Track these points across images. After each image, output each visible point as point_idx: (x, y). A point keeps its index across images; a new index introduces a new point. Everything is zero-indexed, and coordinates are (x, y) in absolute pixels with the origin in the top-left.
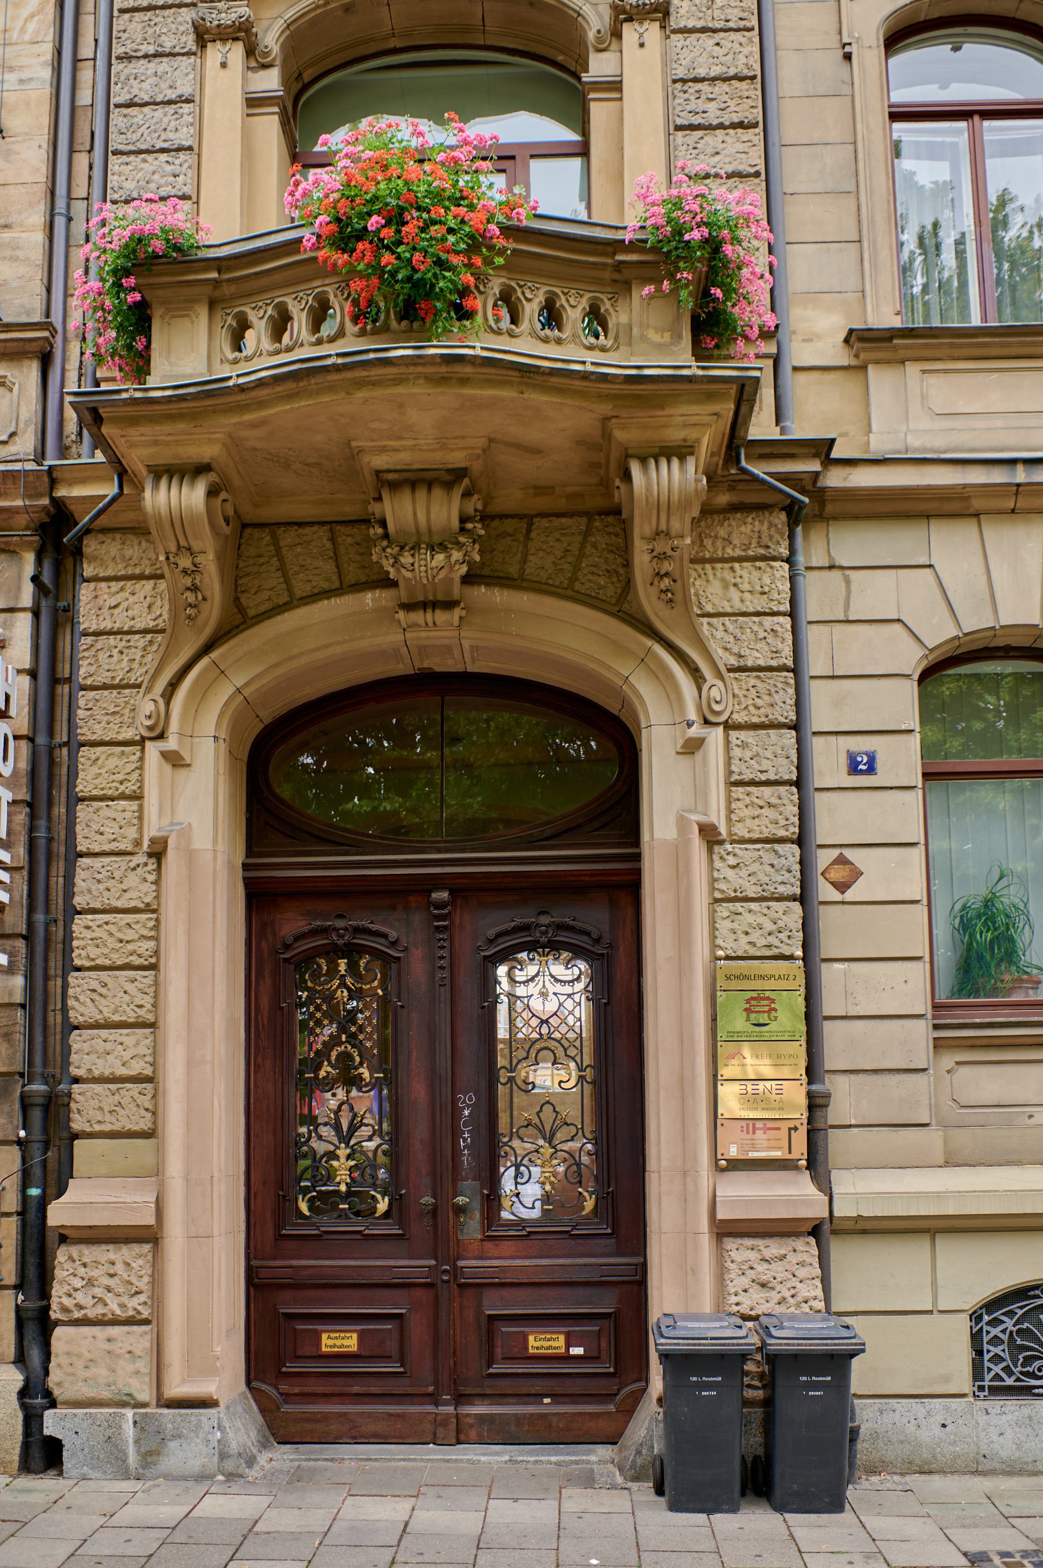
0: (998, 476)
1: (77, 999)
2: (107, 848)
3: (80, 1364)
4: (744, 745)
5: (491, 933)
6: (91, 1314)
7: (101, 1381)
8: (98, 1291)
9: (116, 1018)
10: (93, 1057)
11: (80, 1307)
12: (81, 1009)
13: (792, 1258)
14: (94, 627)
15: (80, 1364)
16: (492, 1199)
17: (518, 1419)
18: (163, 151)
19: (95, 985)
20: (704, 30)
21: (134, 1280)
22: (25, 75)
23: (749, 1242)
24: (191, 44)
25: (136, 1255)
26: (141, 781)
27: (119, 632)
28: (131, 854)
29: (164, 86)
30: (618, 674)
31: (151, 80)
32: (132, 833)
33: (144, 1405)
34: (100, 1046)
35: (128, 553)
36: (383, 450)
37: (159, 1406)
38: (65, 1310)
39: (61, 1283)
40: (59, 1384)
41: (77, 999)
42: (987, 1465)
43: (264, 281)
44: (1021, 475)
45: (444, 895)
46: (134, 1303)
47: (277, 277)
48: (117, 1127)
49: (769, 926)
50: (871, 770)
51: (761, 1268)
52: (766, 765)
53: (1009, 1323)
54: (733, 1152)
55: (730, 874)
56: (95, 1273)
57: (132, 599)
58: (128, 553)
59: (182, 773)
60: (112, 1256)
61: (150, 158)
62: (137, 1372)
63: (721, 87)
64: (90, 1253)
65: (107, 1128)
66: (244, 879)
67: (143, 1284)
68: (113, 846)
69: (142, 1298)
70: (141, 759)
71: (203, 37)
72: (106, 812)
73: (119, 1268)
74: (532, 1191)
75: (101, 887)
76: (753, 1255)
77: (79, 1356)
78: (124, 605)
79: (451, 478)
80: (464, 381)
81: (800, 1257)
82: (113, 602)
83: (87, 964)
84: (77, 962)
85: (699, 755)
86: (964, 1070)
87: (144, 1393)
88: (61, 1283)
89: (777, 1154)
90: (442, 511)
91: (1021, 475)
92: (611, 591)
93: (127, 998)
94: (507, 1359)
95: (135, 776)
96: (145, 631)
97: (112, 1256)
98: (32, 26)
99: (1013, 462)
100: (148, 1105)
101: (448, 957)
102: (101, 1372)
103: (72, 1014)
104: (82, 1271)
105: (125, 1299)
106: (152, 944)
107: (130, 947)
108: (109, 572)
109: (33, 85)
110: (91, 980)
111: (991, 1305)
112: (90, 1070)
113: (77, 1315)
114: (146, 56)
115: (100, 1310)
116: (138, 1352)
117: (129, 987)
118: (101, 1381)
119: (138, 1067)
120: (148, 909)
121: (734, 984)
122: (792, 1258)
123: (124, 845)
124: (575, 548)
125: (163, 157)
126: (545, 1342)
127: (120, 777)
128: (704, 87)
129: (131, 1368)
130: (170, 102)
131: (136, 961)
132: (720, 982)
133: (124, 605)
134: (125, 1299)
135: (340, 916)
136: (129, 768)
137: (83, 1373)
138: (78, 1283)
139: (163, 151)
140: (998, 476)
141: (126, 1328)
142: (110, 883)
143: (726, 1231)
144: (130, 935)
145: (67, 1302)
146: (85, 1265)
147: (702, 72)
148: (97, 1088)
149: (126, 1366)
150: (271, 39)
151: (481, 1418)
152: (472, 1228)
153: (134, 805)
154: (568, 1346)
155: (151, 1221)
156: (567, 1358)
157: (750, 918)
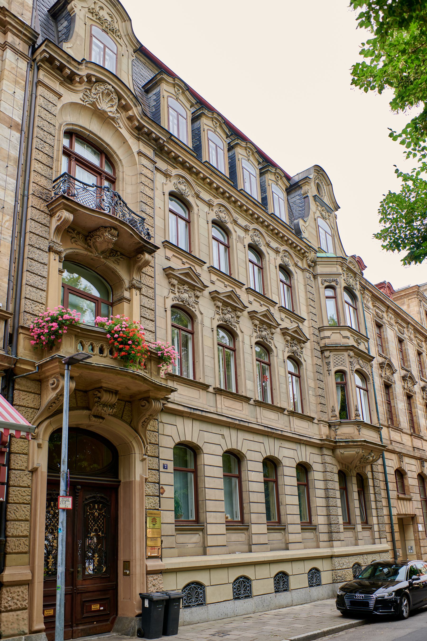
0: (189, 410)
1: (10, 512)
2: (19, 468)
3: (9, 624)
4: (150, 460)
5: (87, 497)
6: (13, 608)
7: (16, 628)
8: (15, 601)
9: (20, 518)
10: (13, 530)
11: (10, 606)
12: (11, 515)
13: (159, 579)
14: (18, 404)
15: (9, 624)
16: (84, 569)
17: (90, 629)
18: (39, 276)
19: (15, 508)
20: (146, 296)
21: (24, 596)
22: (5, 237)
23: (151, 576)
24: (47, 250)
25: (24, 589)
26: (28, 450)
27: (24, 407)
28: (24, 470)
29: (41, 258)
30: (129, 440)
31: (37, 255)
32: (25, 464)
33: (26, 634)
34: (16, 527)
35: (28, 385)
36: (106, 383)
37: (30, 634)
38: (5, 607)
39: (4, 599)
40: (4, 631)
41: (10, 512)
42: (185, 623)
43: (90, 336)
44: (192, 411)
45: (80, 487)
46: (25, 603)
47: (93, 337)
48: (19, 551)
49: (154, 502)
50: (167, 468)
51: (154, 581)
52: (154, 465)
53: (187, 591)
54: (149, 554)
55: (148, 489)
56: (14, 595)
57: (28, 398)
58: (28, 385)
59: (40, 449)
60: (18, 590)
61: (37, 276)
62: (25, 624)
63: (149, 311)
64: (13, 589)
65: (16, 551)
66: (48, 480)
67: (27, 597)
68: (21, 468)
69: (27, 601)
70: (28, 444)
71: (50, 249)
72: (19, 458)
73: (21, 593)
74: (91, 567)
75: (18, 479)
76: (152, 579)
77: (9, 621)
78: (27, 399)
79: (116, 393)
80: (136, 379)
81: (160, 578)
82: (23, 397)
83: (13, 502)
84: (10, 501)
85: (144, 462)
86: (178, 535)
87: (27, 631)
88: (4, 599)
89: (156, 555)
90: (113, 399)
91: (192, 411)
92: (129, 420)
93: (23, 513)
94: (87, 612)
95: (27, 448)
96: (31, 408)
97: (18, 590)
98: (7, 224)
99: (191, 408)
100: (28, 544)
101: (407, 550)
102: (16, 626)
103: (8, 516)
104: (10, 595)
105: (22, 602)
106: (30, 497)
107: (24, 498)
108: (22, 389)
109: (6, 241)
110: (14, 507)
111: (184, 588)
112: (12, 534)
113: (9, 609)
114: (36, 248)
115: (15, 606)
116: (25, 618)
117: (24, 509)
118: (16, 628)
119: (26, 533)
120: (29, 487)
121: (150, 515)
122: (159, 579)
123: (23, 468)
124: (123, 408)
125: (40, 277)
126: (95, 607)
127: (23, 448)
128: (146, 309)
129: (23, 623)
130: (42, 263)
131: (26, 502)
132: (148, 515)
133: (27, 399)
134: (22, 602)
135: (55, 490)
136: (25, 446)
137: (10, 627)
138: (9, 599)
139: (39, 276)
140: (189, 410)
141: (21, 611)
142: (20, 478)
143: (149, 573)
144: (24, 494)
145: (6, 605)
146: (11, 593)
147: (146, 306)
148: (14, 539)
149: (22, 623)
150: (63, 255)
151: (81, 629)
152: (80, 577)
153: (26, 457)
154: (100, 607)
155: (30, 578)
156: (99, 610)
157: (151, 500)
